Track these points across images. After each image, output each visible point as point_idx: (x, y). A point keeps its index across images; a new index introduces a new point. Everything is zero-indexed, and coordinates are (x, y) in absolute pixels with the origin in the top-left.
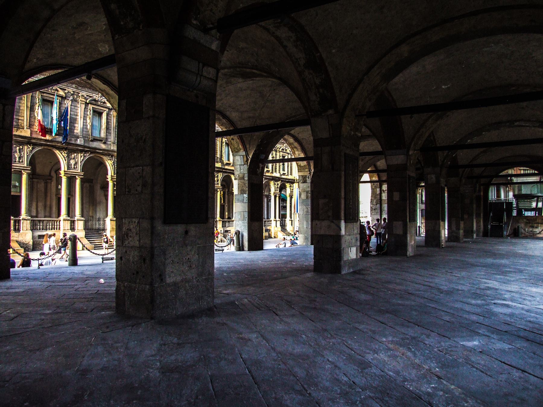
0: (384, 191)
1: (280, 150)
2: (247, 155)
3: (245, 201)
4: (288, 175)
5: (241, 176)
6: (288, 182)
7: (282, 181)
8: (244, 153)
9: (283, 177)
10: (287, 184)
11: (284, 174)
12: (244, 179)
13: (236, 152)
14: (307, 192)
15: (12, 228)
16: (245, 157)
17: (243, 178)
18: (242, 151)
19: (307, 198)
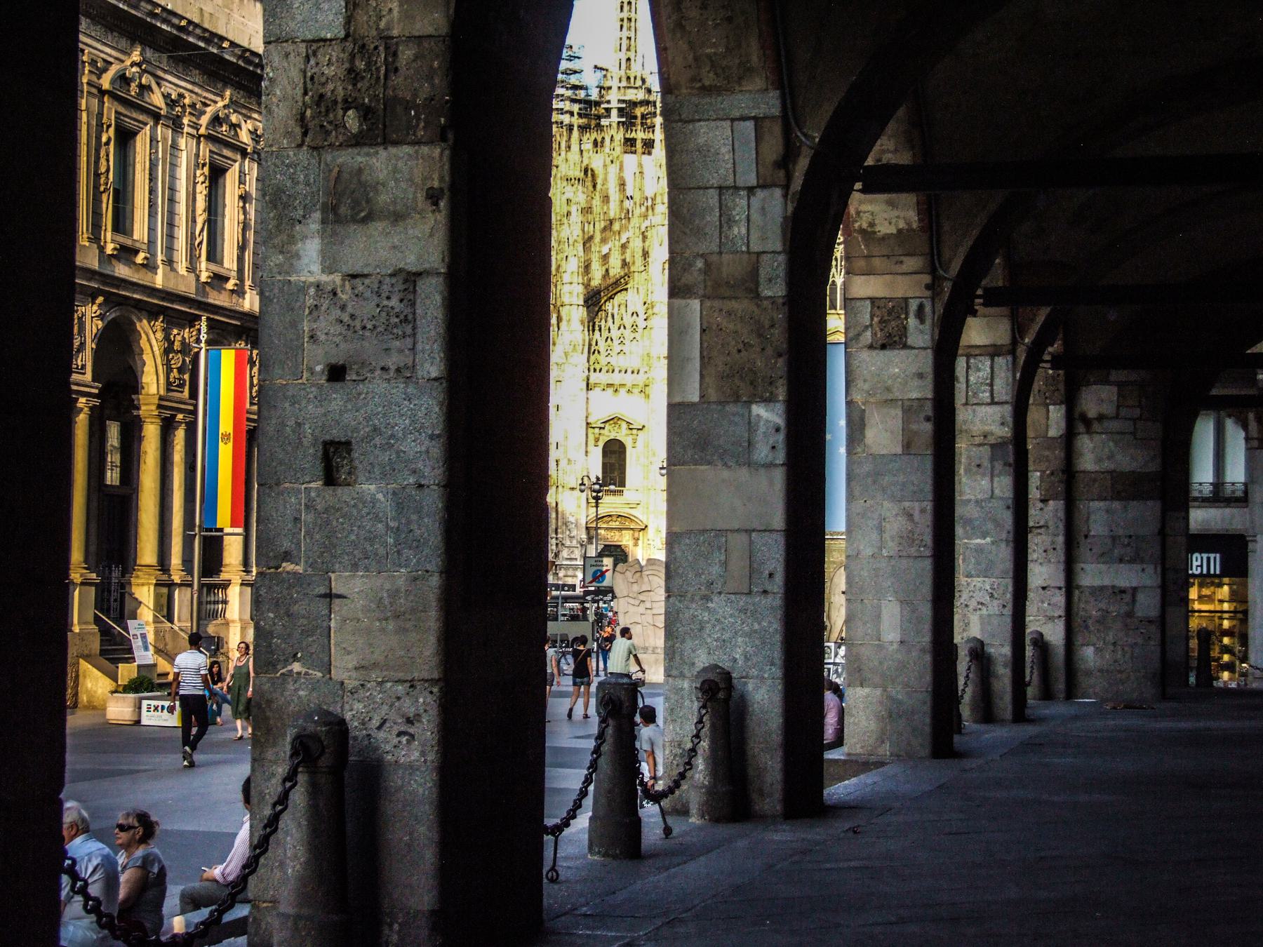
0: (1087, 422)
1: (105, 82)
2: (790, 119)
3: (762, 452)
4: (150, 266)
5: (731, 266)
6: (153, 313)
7: (112, 301)
8: (771, 104)
9: (122, 271)
10: (143, 325)
11: (126, 253)
12: (755, 295)
13: (707, 90)
14: (909, 410)
15: (251, 648)
16: (777, 129)
17: (750, 284)
18: (759, 83)
19: (907, 446)
